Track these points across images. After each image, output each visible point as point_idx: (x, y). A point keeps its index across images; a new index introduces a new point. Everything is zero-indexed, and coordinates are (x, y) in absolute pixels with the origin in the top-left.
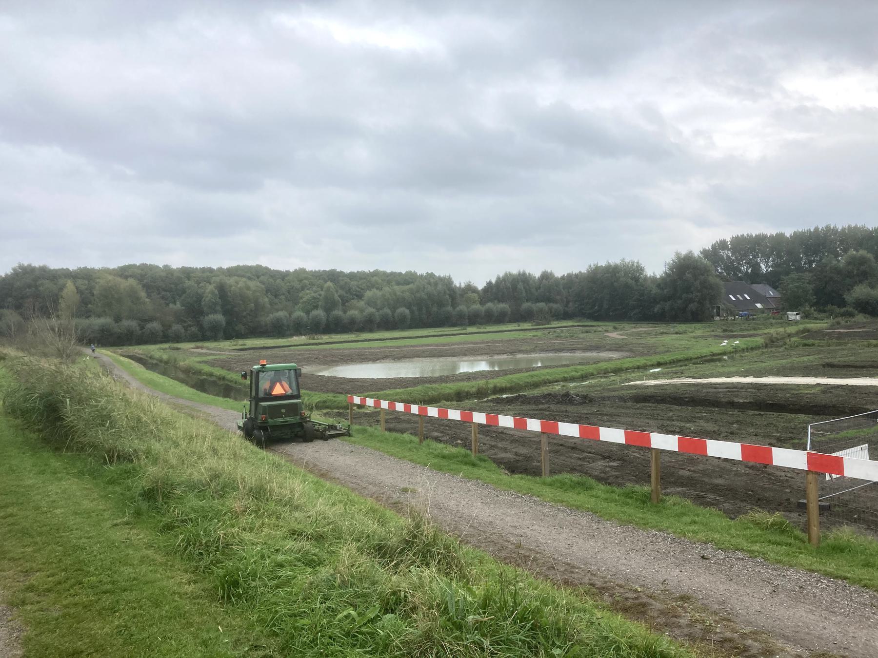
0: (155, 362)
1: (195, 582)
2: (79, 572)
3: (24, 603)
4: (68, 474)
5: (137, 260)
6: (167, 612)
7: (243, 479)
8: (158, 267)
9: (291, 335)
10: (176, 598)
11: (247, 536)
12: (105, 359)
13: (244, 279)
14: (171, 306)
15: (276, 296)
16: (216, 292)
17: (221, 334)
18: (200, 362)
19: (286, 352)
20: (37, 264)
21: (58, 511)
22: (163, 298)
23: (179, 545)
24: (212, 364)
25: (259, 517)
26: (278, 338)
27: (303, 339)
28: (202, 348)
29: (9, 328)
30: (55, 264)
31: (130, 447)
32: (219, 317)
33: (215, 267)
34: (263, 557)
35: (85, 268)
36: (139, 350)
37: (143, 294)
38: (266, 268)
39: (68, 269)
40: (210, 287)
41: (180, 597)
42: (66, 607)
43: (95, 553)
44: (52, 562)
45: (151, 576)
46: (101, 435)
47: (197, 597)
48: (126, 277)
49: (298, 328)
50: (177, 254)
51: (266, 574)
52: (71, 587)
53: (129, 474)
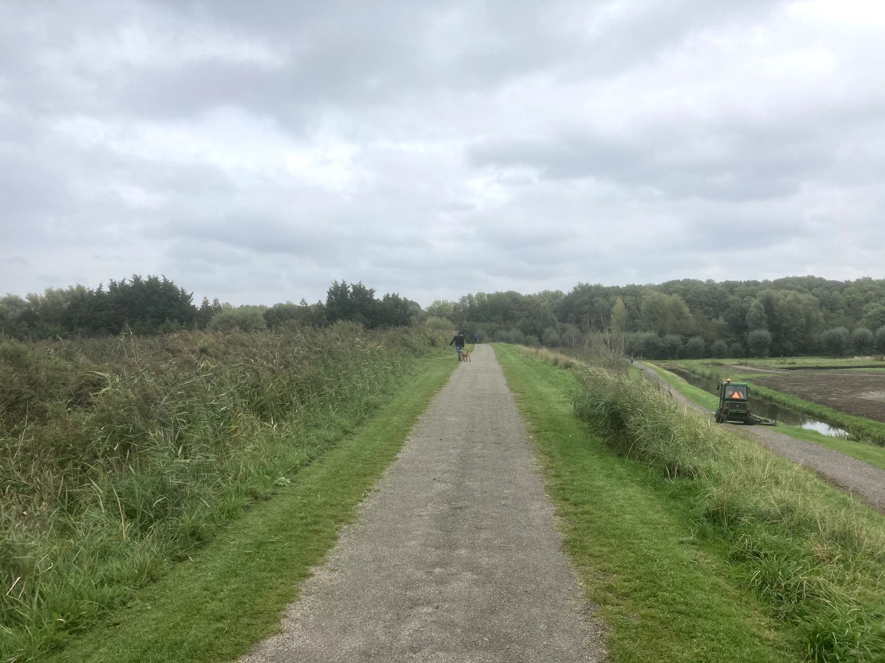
0: (697, 377)
1: (777, 629)
2: (652, 584)
3: (605, 602)
4: (632, 481)
5: (680, 275)
6: (748, 654)
7: (823, 520)
8: (701, 282)
9: (852, 355)
10: (756, 640)
11: (835, 589)
12: (650, 371)
13: (793, 292)
14: (714, 320)
15: (832, 310)
16: (762, 306)
17: (767, 351)
18: (745, 380)
19: (846, 373)
20: (593, 283)
21: (627, 517)
22: (705, 312)
23: (754, 581)
24: (757, 382)
25: (847, 568)
26: (835, 357)
27: (868, 359)
28: (746, 365)
29: (570, 338)
30: (607, 283)
31: (691, 463)
32: (765, 333)
33: (760, 280)
34: (860, 621)
35: (633, 286)
36: (681, 364)
37: (686, 310)
38: (821, 279)
39: (618, 287)
40: (755, 302)
41: (761, 641)
42: (643, 617)
43: (666, 567)
44: (627, 567)
45: (725, 608)
46: (661, 448)
47: (780, 648)
48: (670, 293)
49: (861, 347)
50: (716, 269)
51: (866, 643)
52: (647, 597)
53: (691, 491)
